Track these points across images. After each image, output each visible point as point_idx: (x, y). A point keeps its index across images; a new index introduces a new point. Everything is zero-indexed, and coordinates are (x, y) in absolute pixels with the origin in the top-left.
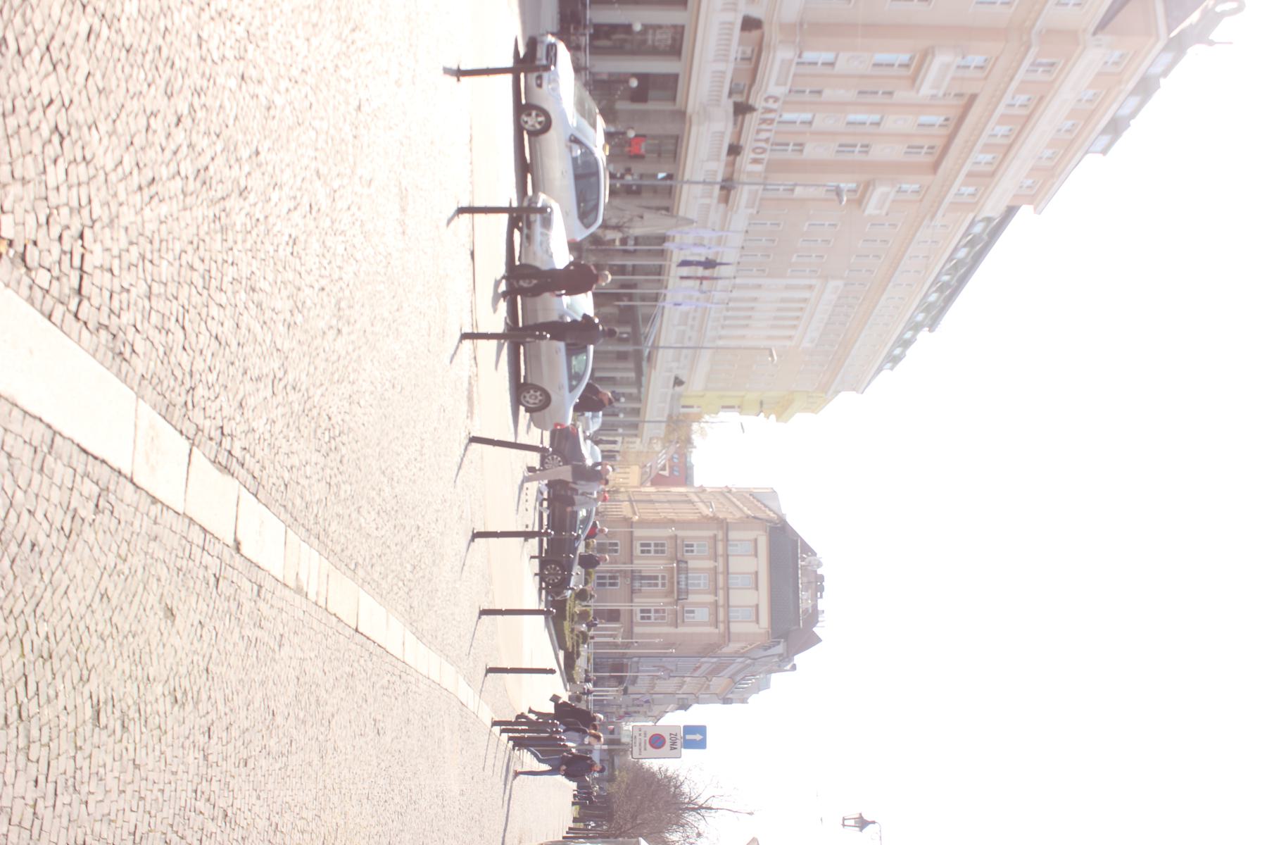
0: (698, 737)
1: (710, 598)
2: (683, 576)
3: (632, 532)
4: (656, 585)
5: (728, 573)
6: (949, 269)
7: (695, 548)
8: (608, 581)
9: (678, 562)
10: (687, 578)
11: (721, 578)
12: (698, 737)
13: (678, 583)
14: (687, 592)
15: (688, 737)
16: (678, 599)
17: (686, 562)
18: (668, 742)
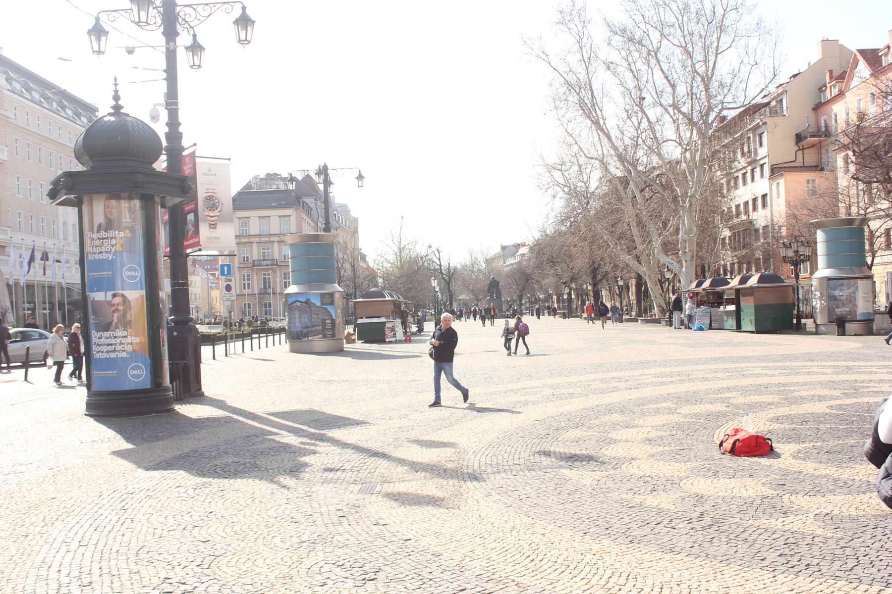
0: (226, 268)
1: (276, 245)
2: (263, 263)
3: (248, 295)
4: (269, 279)
5: (260, 235)
6: (48, 103)
7: (246, 256)
8: (268, 309)
9: (254, 266)
10: (264, 260)
11: (263, 239)
12: (226, 268)
13: (267, 265)
14: (273, 260)
15: (226, 273)
16: (277, 265)
17: (254, 261)
18: (229, 283)
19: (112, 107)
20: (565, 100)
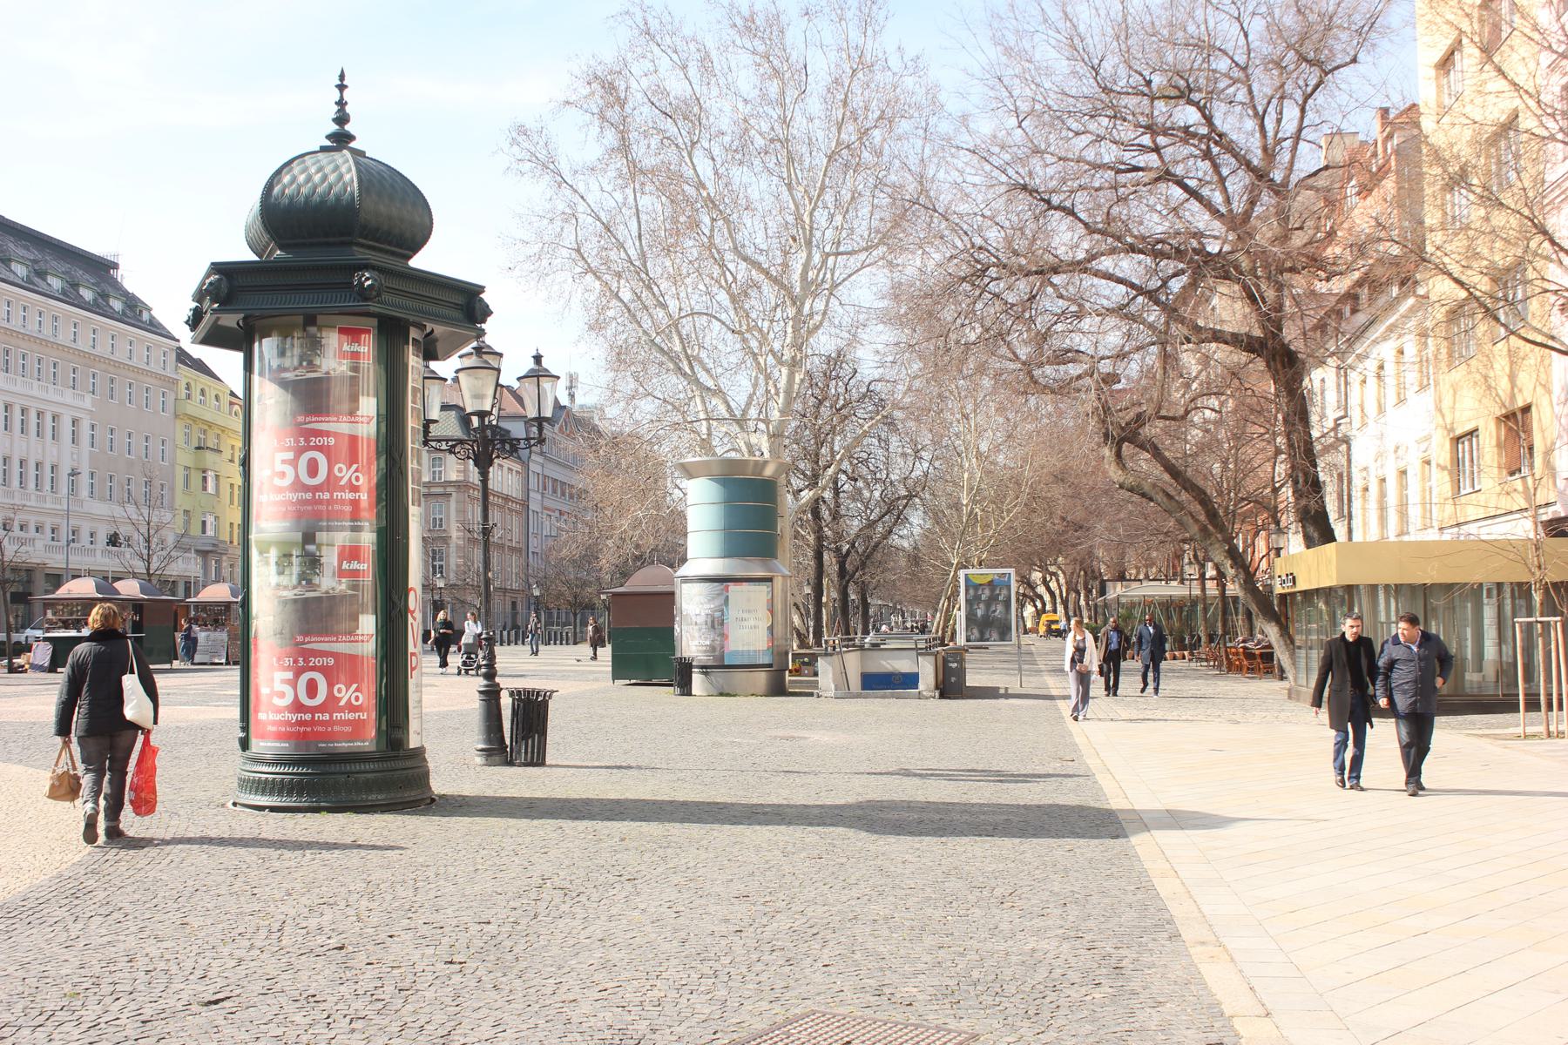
7: (438, 517)
19: (329, 137)
20: (1359, 32)
